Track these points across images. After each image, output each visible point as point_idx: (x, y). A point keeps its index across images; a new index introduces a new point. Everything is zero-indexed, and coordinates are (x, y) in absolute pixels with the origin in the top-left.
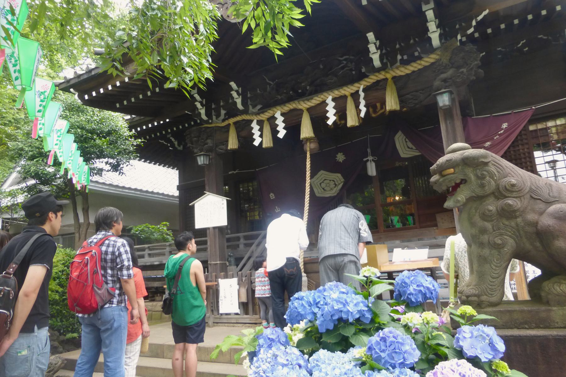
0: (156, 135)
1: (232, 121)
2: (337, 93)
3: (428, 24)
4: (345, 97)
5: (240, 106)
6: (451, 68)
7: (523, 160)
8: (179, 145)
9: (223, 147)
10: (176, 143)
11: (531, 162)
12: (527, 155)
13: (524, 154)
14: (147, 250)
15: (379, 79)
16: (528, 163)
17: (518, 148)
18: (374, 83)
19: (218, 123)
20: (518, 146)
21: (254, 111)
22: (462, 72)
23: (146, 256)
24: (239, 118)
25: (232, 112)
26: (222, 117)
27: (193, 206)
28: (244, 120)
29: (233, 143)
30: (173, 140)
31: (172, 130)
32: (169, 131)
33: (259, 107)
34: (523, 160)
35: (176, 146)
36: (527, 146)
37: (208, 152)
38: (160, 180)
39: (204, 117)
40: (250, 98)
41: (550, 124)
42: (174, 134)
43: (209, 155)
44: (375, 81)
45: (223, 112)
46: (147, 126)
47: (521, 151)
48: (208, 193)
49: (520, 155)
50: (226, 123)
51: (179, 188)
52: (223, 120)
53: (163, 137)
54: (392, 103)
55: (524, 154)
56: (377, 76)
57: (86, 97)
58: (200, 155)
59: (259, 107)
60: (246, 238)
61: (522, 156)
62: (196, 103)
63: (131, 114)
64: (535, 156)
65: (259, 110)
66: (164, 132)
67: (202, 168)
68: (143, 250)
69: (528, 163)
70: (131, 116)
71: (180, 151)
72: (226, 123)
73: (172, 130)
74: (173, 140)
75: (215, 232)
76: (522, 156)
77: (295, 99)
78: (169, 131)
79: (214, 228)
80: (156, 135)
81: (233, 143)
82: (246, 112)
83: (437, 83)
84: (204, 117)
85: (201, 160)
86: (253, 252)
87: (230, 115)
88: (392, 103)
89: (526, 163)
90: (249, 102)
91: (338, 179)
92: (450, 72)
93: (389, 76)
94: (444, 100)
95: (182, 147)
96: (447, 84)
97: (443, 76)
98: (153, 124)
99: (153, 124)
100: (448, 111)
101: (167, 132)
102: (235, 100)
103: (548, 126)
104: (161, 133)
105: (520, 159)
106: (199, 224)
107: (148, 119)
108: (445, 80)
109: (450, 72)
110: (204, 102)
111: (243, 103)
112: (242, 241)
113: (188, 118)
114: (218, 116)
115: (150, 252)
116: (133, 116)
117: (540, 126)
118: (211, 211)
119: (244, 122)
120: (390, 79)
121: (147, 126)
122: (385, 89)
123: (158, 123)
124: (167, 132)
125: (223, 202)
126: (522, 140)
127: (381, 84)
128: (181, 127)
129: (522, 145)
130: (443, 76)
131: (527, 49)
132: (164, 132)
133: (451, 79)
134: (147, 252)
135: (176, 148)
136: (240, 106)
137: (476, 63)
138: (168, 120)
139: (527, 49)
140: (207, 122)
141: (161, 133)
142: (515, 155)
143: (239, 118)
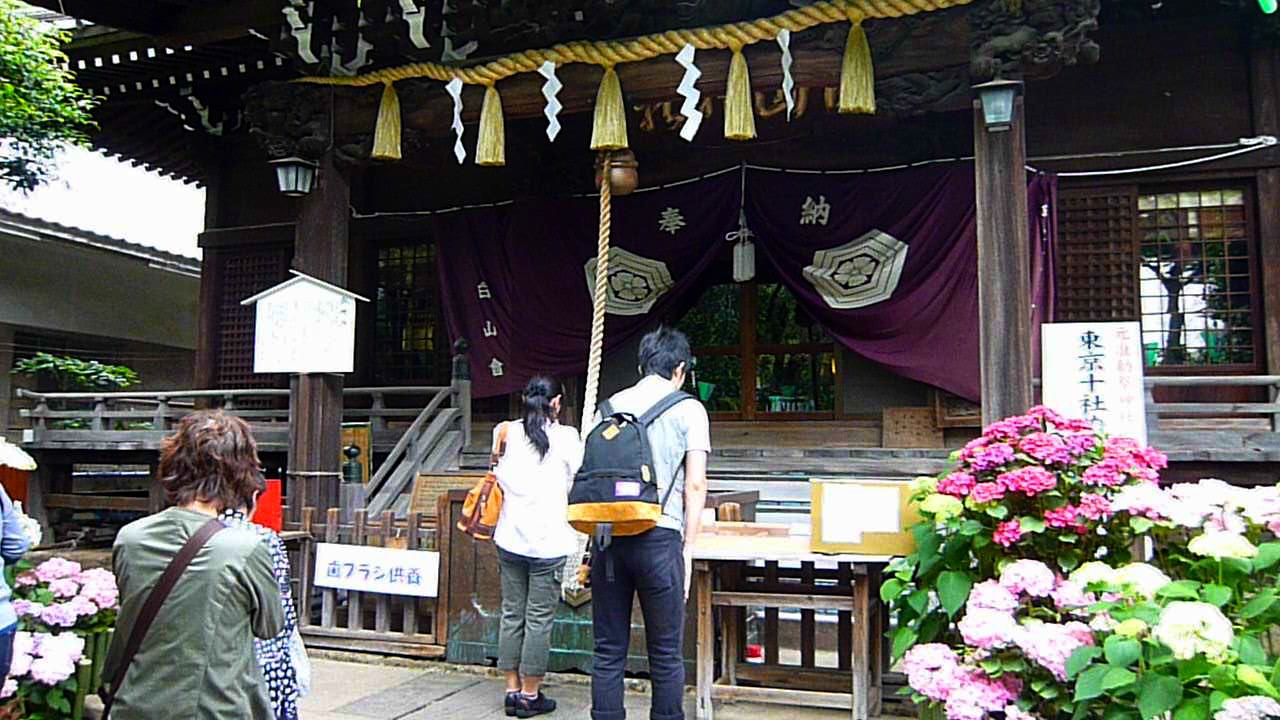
0: (147, 85)
1: (389, 77)
2: (707, 38)
3: (289, 19)
4: (728, 53)
5: (418, 38)
6: (1021, 24)
7: (1114, 281)
8: (213, 121)
9: (358, 149)
10: (205, 114)
11: (1131, 289)
12: (1124, 268)
13: (1119, 267)
14: (99, 407)
15: (826, 20)
16: (1124, 291)
17: (1105, 251)
18: (810, 28)
19: (345, 76)
20: (1106, 244)
21: (456, 56)
22: (1053, 39)
23: (98, 423)
24: (411, 72)
25: (393, 48)
26: (360, 61)
27: (254, 305)
28: (425, 79)
29: (387, 143)
30: (197, 104)
31: (198, 76)
32: (189, 77)
33: (472, 47)
34: (1114, 281)
35: (205, 122)
36: (1127, 248)
37: (309, 158)
38: (157, 213)
39: (306, 54)
40: (447, 17)
41: (1187, 201)
42: (199, 88)
43: (313, 168)
44: (814, 23)
45: (363, 47)
46: (125, 57)
47: (1112, 257)
48: (302, 275)
49: (1108, 267)
50: (371, 79)
51: (202, 240)
52: (363, 71)
53: (167, 93)
54: (856, 94)
55: (1119, 267)
56: (822, 10)
57: (82, 65)
58: (286, 165)
59: (472, 47)
60: (390, 401)
61: (1114, 271)
62: (287, 10)
63: (77, 16)
64: (1142, 277)
65: (469, 56)
66: (172, 80)
67: (292, 204)
68: (89, 404)
69: (1124, 291)
70: (78, 23)
71: (214, 136)
72: (371, 79)
73: (198, 76)
74: (197, 104)
75: (312, 389)
76: (1114, 271)
77: (578, 40)
78: (189, 77)
79: (312, 376)
80: (147, 85)
81: (387, 143)
82: (432, 55)
83: (981, 60)
84: (306, 54)
85: (288, 181)
86: (409, 445)
87: (381, 59)
88: (856, 94)
89: (1119, 289)
90: (445, 31)
91: (656, 275)
92: (1020, 36)
93: (856, 15)
94: (998, 109)
95: (220, 128)
96: (1008, 66)
97: (1000, 42)
98: (143, 54)
99: (143, 54)
100: (999, 138)
101: (181, 80)
102: (293, 33)
103: (1182, 205)
104: (164, 82)
105: (1109, 278)
106: (266, 360)
107: (125, 35)
108: (1003, 55)
109: (1020, 36)
110: (311, 12)
111: (429, 30)
112: (377, 407)
113: (264, 51)
114: (348, 55)
115: (107, 414)
116: (85, 22)
117: (1164, 203)
118: (306, 326)
119: (426, 85)
120: (857, 25)
121: (125, 57)
122: (841, 52)
123: (160, 51)
124: (181, 80)
125: (344, 306)
126: (1117, 231)
127: (830, 34)
128: (242, 68)
129: (1118, 243)
130: (1000, 42)
131: (1159, 5)
132: (172, 80)
133: (1019, 52)
134: (99, 412)
135: (204, 128)
136: (418, 38)
137: (1088, 22)
138: (188, 48)
139: (1159, 5)
140: (311, 69)
141: (164, 82)
142: (1096, 266)
143: (411, 72)
